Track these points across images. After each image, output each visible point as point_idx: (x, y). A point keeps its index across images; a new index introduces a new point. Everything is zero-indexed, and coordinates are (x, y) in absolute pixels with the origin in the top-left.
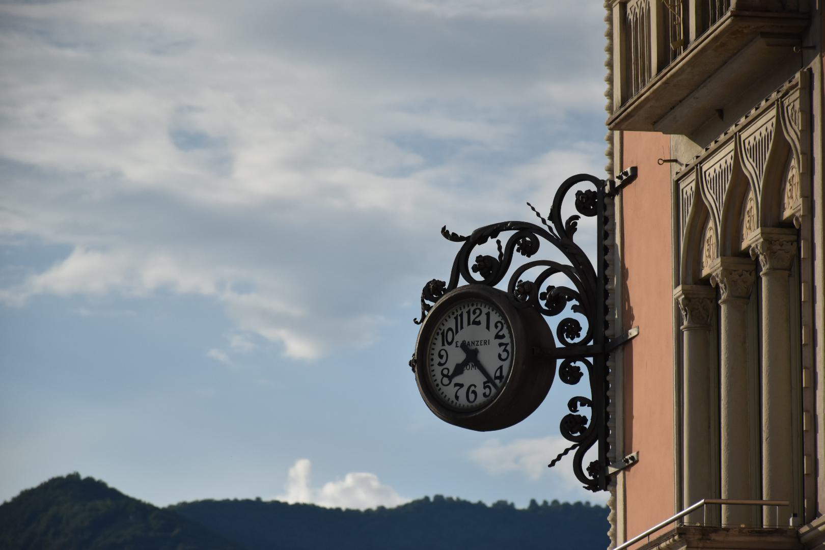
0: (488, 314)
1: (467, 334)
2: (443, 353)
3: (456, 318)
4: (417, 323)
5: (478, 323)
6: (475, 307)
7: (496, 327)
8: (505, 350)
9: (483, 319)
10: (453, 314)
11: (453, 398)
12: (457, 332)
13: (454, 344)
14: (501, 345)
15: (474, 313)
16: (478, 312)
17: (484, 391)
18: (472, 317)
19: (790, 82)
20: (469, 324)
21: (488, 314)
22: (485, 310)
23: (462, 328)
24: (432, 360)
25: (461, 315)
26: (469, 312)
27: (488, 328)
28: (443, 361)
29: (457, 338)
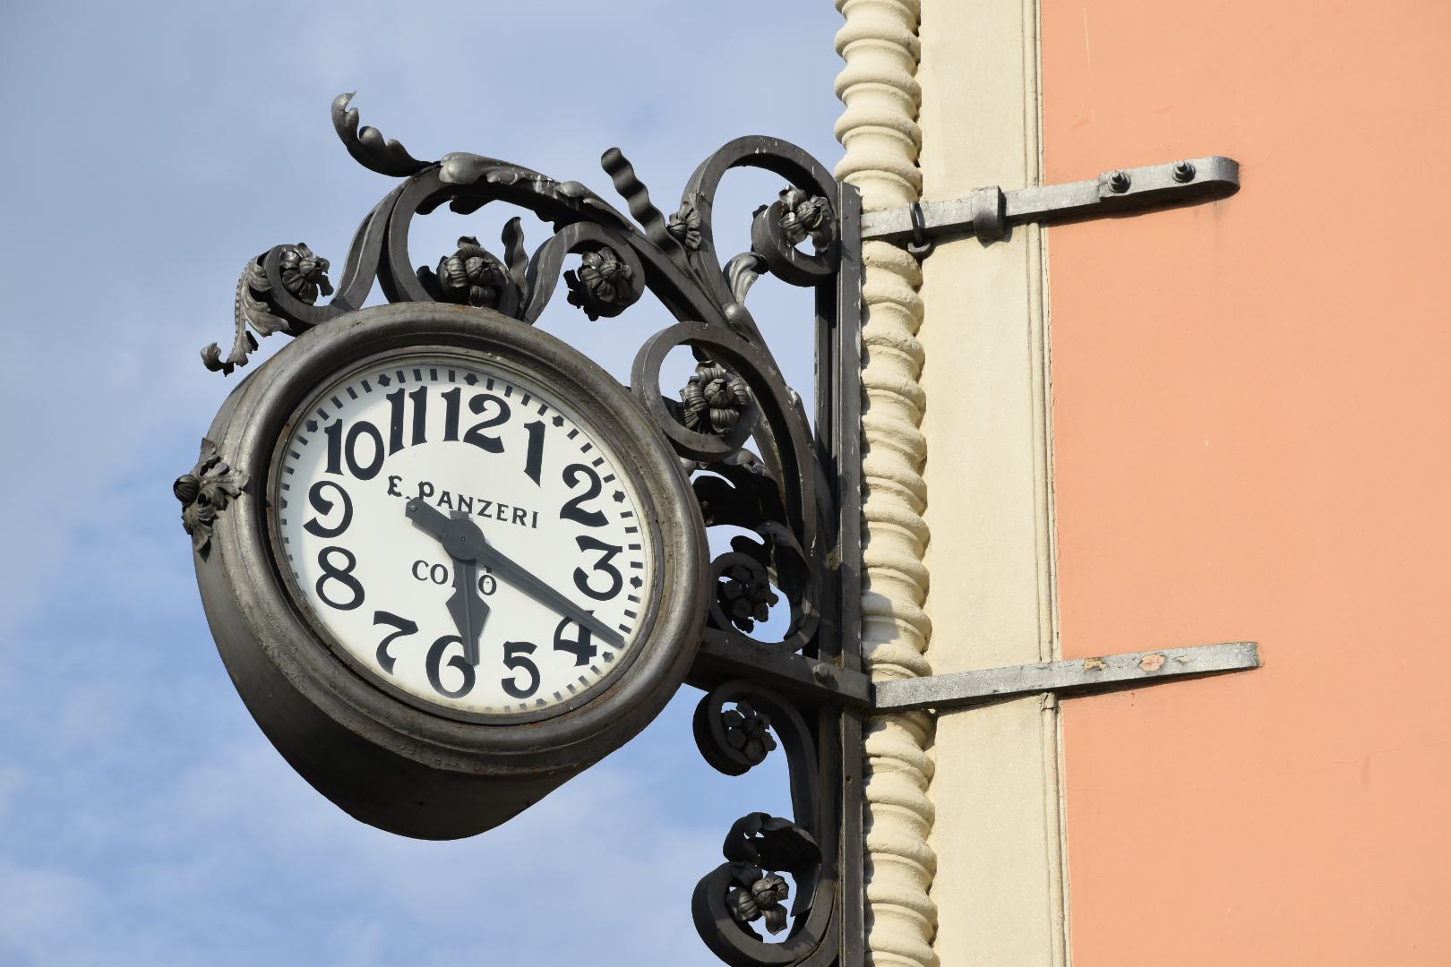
0: (536, 431)
1: (438, 464)
2: (327, 494)
3: (397, 400)
4: (213, 363)
5: (495, 446)
6: (480, 389)
7: (569, 477)
8: (603, 565)
9: (514, 436)
10: (384, 381)
11: (499, 582)
12: (396, 445)
13: (381, 480)
14: (586, 543)
15: (477, 405)
16: (492, 410)
17: (508, 673)
18: (467, 420)
19: (523, 706)
20: (451, 434)
21: (536, 431)
22: (524, 413)
23: (419, 437)
24: (434, 377)
25: (420, 398)
26: (453, 399)
27: (534, 469)
28: (331, 521)
29: (391, 464)
